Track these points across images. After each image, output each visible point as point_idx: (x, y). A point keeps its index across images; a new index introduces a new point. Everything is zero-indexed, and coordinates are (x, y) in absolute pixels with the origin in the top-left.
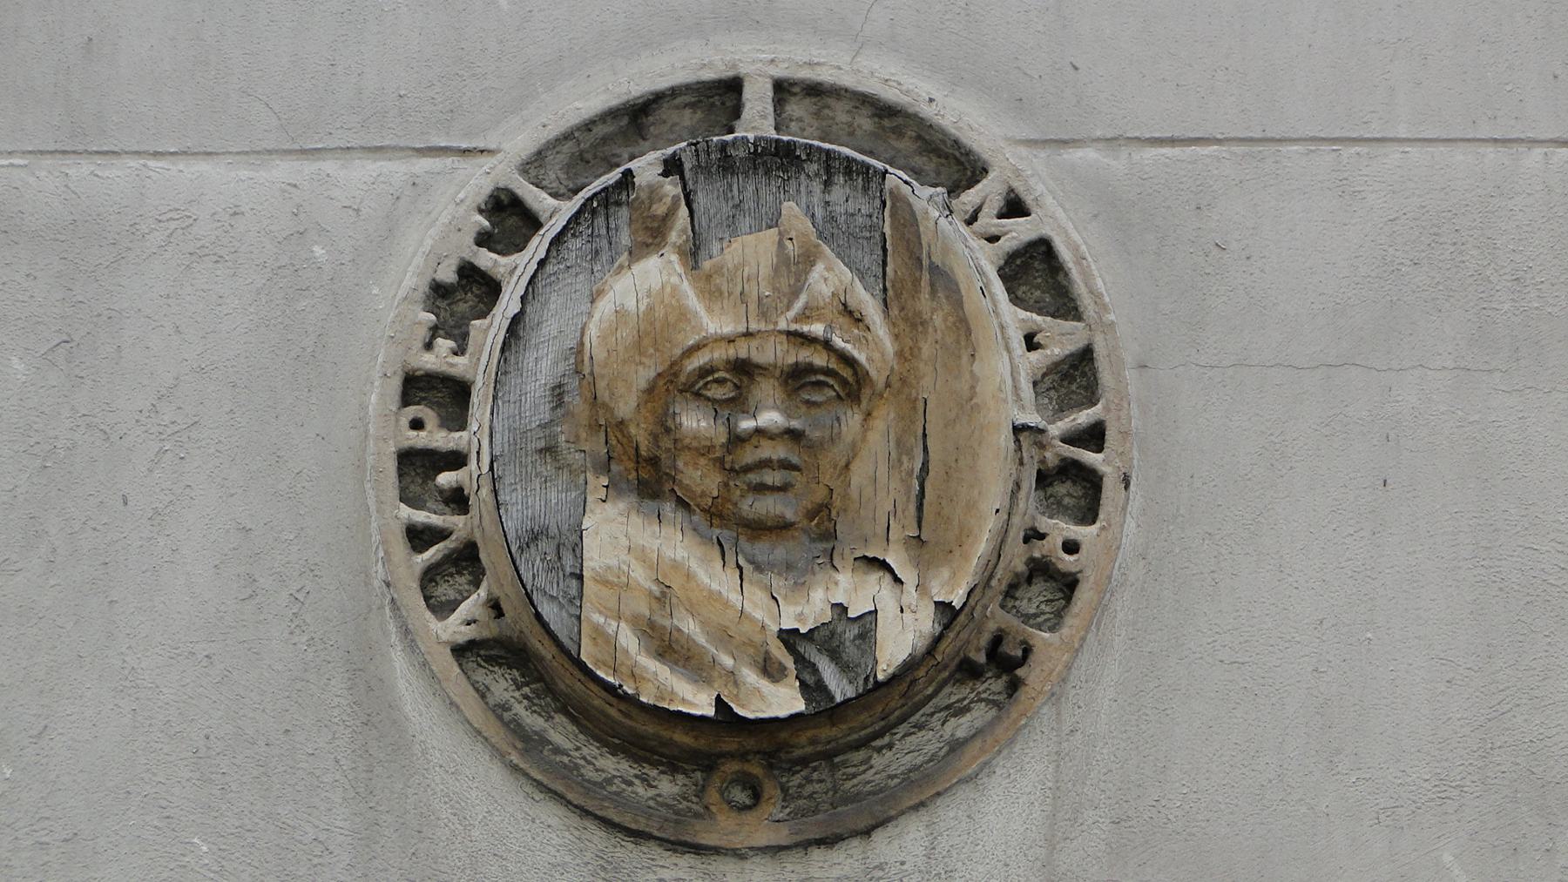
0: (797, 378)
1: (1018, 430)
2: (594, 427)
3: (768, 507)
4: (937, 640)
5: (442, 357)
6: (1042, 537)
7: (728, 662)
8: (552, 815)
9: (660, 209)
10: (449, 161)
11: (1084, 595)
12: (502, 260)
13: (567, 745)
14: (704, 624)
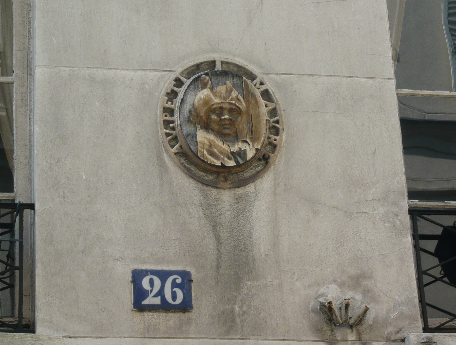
0: (231, 111)
1: (267, 120)
2: (197, 117)
3: (227, 131)
4: (256, 154)
5: (169, 105)
6: (270, 138)
7: (222, 157)
8: (192, 181)
9: (206, 81)
10: (168, 72)
11: (278, 148)
12: (178, 89)
13: (193, 170)
14: (218, 150)
